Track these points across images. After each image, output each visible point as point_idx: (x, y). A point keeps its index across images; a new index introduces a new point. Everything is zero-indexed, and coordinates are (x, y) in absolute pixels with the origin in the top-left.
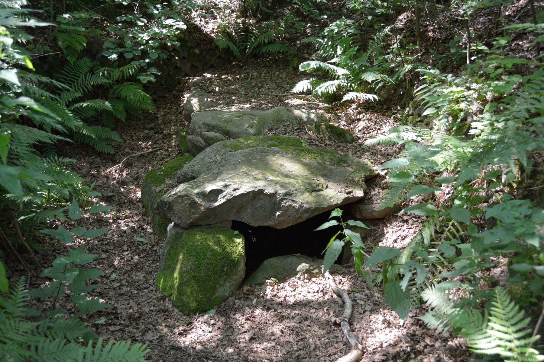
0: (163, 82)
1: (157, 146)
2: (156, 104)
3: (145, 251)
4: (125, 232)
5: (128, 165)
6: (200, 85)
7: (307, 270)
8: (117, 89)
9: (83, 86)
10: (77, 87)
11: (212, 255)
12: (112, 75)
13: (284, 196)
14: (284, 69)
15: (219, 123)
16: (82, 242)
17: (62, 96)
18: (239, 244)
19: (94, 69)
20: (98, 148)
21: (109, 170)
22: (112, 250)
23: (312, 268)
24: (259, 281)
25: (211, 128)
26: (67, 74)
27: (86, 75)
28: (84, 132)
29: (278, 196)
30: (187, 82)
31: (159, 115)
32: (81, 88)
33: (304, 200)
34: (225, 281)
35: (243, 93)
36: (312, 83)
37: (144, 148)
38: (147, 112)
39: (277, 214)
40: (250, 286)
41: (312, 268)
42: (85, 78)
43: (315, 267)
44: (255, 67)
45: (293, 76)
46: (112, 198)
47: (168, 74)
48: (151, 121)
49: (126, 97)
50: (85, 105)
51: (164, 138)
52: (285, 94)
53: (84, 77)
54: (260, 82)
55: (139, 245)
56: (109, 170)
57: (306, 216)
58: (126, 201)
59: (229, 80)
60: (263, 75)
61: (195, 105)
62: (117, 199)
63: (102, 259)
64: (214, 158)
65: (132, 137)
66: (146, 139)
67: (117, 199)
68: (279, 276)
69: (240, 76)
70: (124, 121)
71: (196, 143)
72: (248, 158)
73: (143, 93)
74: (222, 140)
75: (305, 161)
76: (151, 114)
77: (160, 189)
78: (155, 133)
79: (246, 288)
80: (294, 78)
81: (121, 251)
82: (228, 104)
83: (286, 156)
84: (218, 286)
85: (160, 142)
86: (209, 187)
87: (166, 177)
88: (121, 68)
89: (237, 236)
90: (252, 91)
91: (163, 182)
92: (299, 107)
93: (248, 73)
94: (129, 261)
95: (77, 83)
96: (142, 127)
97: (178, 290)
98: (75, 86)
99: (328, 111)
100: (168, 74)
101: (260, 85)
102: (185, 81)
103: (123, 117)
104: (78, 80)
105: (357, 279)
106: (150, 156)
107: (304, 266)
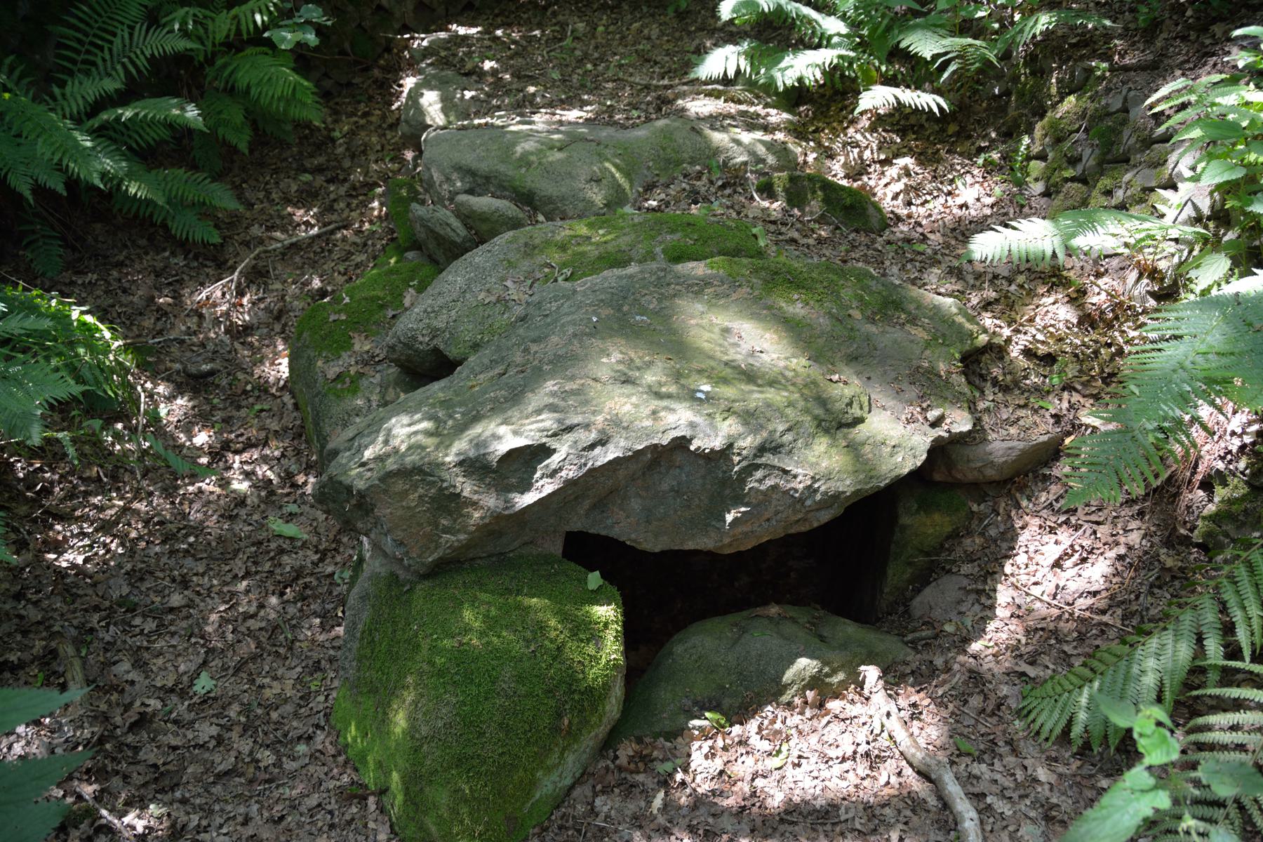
0: (347, 45)
1: (335, 217)
2: (331, 104)
3: (298, 573)
4: (241, 501)
5: (257, 276)
6: (443, 54)
7: (813, 678)
8: (225, 66)
9: (125, 60)
10: (109, 63)
11: (520, 679)
12: (211, 28)
13: (755, 456)
14: (653, 15)
15: (502, 168)
16: (113, 546)
17: (68, 90)
18: (606, 625)
19: (162, 14)
20: (177, 228)
21: (204, 295)
22: (203, 575)
23: (826, 669)
24: (667, 725)
25: (480, 181)
26: (82, 26)
27: (132, 28)
28: (132, 190)
29: (736, 459)
30: (407, 47)
31: (337, 134)
32: (119, 67)
33: (818, 467)
34: (562, 754)
35: (556, 75)
36: (750, 56)
37: (299, 225)
38: (308, 125)
39: (729, 518)
40: (639, 740)
41: (826, 669)
42: (131, 35)
43: (836, 665)
44: (579, 9)
45: (677, 35)
46: (210, 379)
47: (359, 26)
48: (319, 147)
49: (249, 87)
50: (128, 114)
51: (351, 196)
52: (666, 82)
53: (126, 36)
54: (596, 47)
55: (281, 551)
56: (204, 295)
57: (825, 516)
58: (249, 387)
59: (514, 42)
60: (601, 29)
61: (430, 109)
62: (224, 382)
63: (172, 610)
64: (498, 290)
65: (268, 193)
66: (306, 198)
67: (224, 382)
68: (726, 702)
69: (543, 31)
70: (246, 151)
71: (438, 229)
72: (619, 310)
73: (293, 77)
74: (515, 224)
75: (791, 309)
76: (318, 129)
77: (337, 370)
78: (328, 181)
79: (626, 751)
80: (681, 38)
81: (228, 578)
82: (519, 106)
83: (734, 296)
84: (539, 774)
85: (342, 205)
86: (506, 438)
87: (355, 330)
88: (234, 11)
89: (597, 597)
90: (579, 71)
91: (347, 345)
92: (716, 121)
93: (563, 25)
94: (253, 616)
95: (110, 50)
96: (294, 166)
97: (407, 792)
98: (104, 60)
99: (799, 132)
100: (359, 26)
101: (596, 55)
102: (403, 43)
103: (242, 142)
104: (111, 42)
105: (966, 702)
106: (316, 248)
107: (805, 665)
